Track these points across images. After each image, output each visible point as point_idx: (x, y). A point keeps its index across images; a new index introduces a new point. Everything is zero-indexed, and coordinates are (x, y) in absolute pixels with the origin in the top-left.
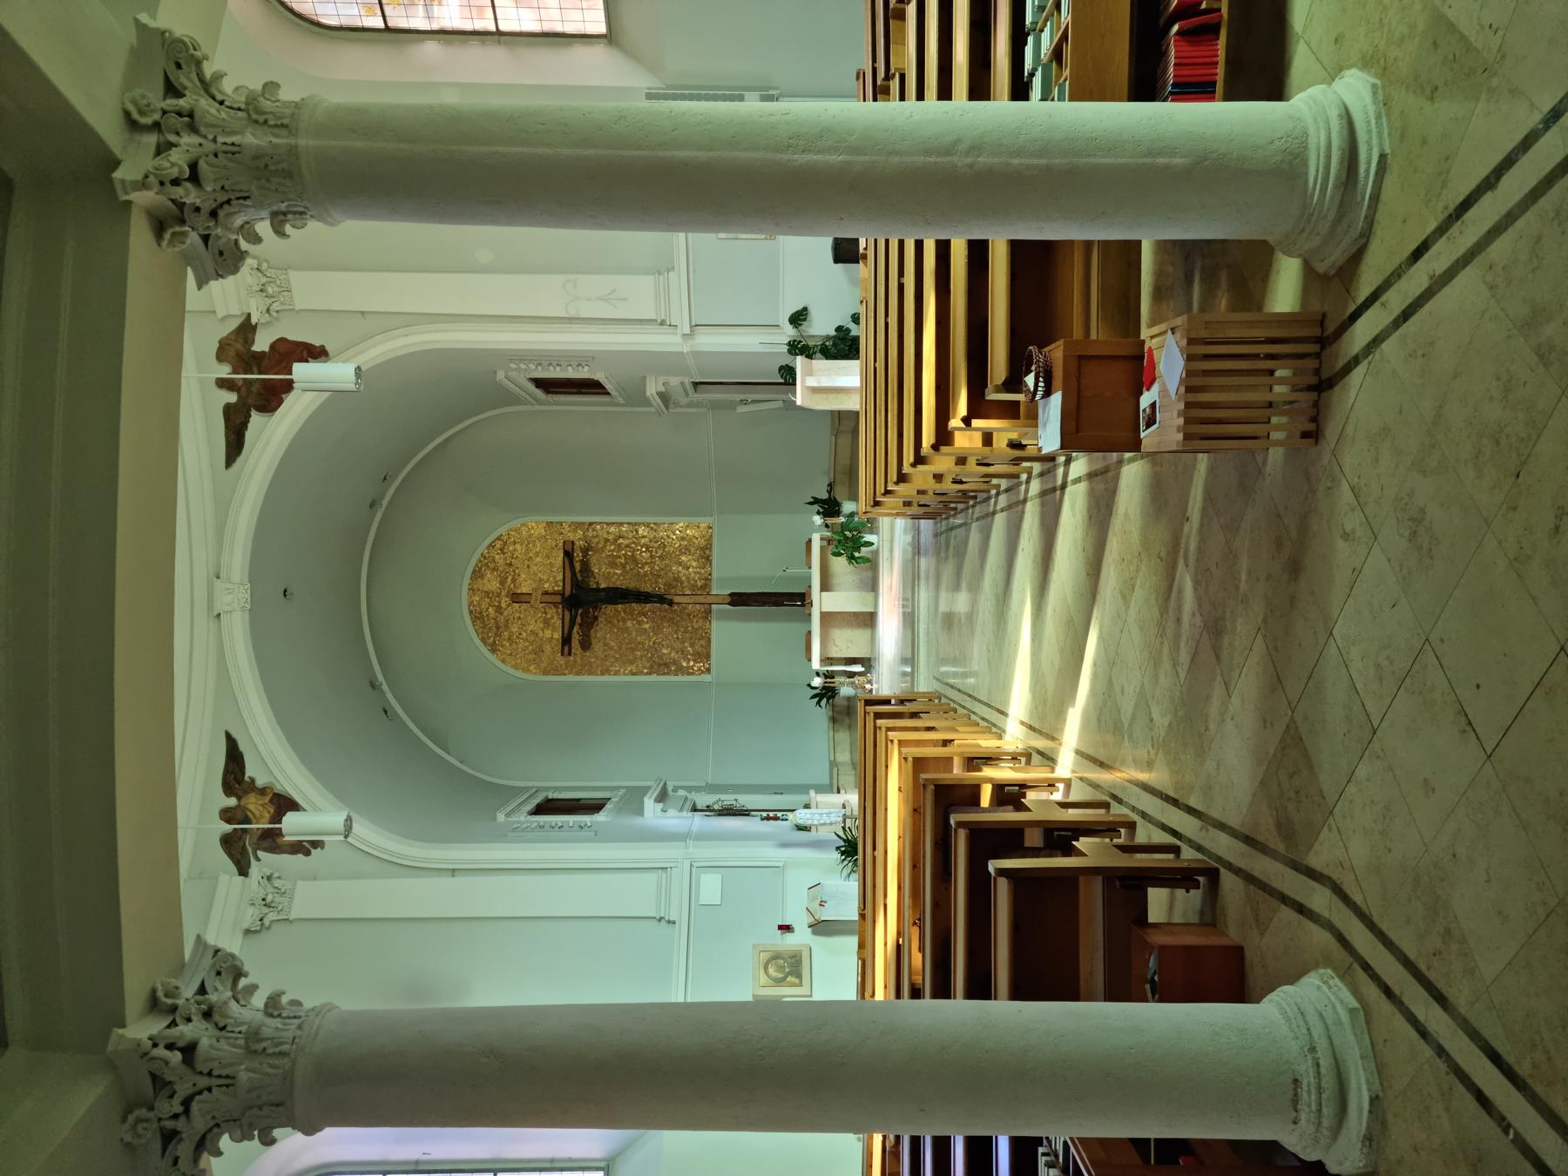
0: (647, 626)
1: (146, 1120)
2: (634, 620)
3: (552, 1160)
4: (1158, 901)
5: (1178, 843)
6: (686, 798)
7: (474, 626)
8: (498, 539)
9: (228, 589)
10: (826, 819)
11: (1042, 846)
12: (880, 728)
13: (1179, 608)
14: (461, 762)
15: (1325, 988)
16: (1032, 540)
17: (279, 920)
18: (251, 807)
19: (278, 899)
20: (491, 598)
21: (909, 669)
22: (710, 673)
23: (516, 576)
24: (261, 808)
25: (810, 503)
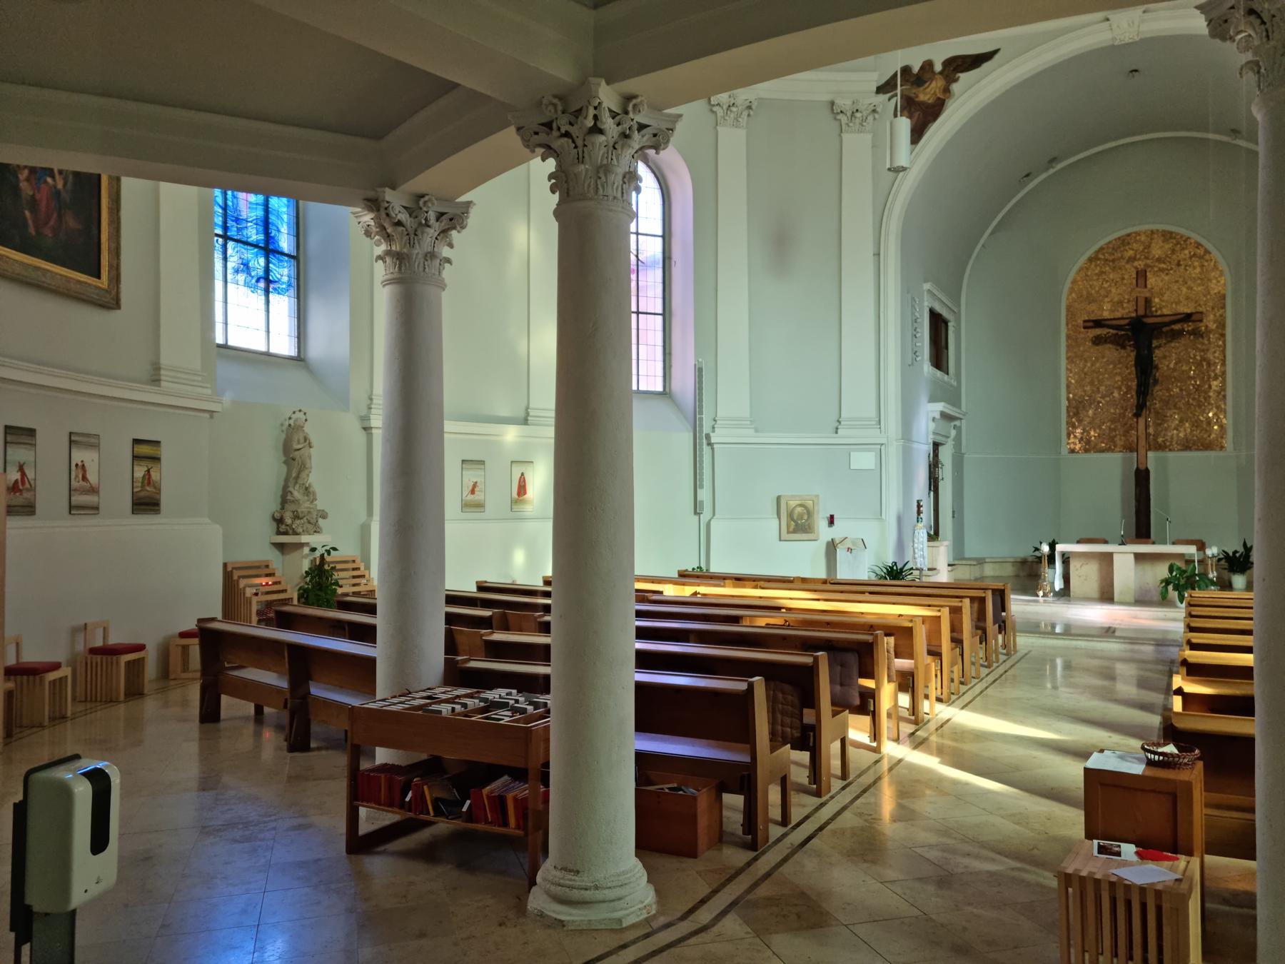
0: (1116, 394)
1: (556, 111)
2: (1122, 383)
3: (670, 354)
4: (734, 801)
5: (790, 826)
6: (948, 437)
7: (1115, 240)
8: (1207, 252)
9: (1133, 23)
10: (918, 554)
11: (804, 722)
12: (961, 601)
13: (977, 857)
14: (983, 246)
15: (641, 906)
16: (1115, 745)
17: (841, 125)
18: (934, 84)
19: (858, 121)
20: (1143, 251)
21: (1058, 630)
22: (1069, 453)
23: (1167, 272)
24: (932, 92)
25: (1245, 544)
